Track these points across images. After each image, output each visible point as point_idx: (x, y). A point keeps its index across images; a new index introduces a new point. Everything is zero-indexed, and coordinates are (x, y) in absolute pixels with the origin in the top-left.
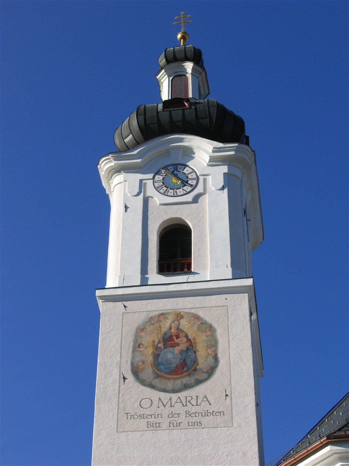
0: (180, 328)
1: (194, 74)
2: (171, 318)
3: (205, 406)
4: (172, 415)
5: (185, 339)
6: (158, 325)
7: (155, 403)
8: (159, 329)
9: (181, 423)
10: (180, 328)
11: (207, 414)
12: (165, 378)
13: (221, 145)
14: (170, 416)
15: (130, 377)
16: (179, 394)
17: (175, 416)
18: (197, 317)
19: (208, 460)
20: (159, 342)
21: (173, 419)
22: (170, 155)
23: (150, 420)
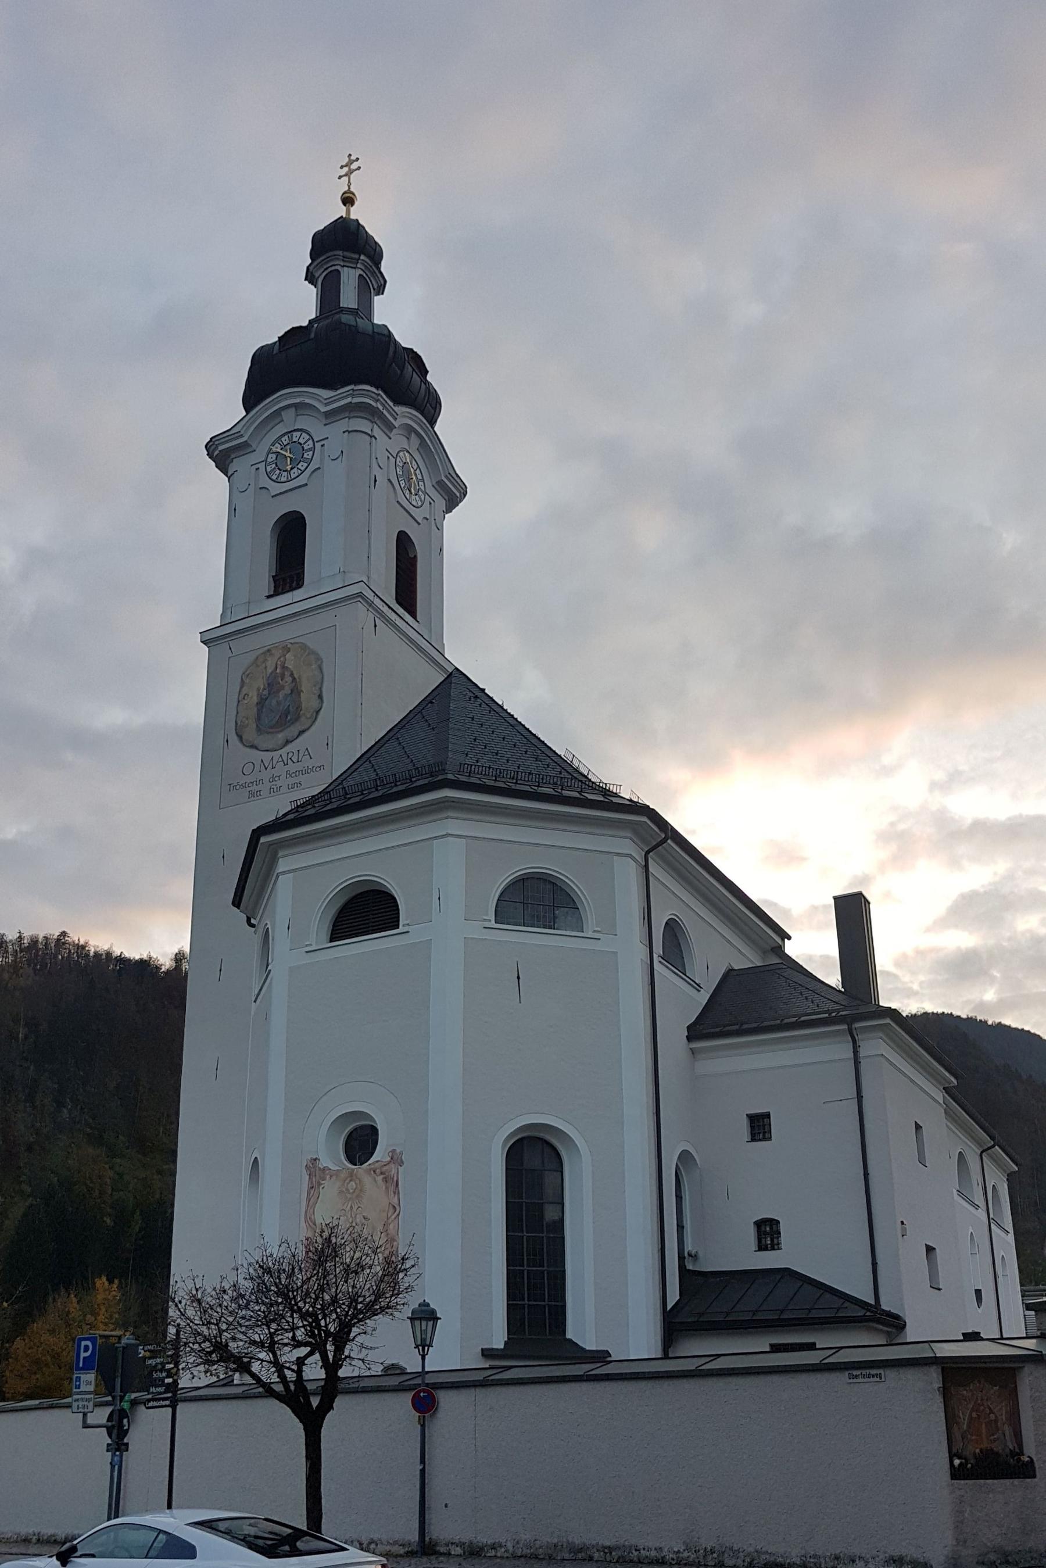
0: (286, 665)
1: (381, 292)
2: (277, 654)
3: (307, 763)
4: (273, 779)
5: (291, 679)
6: (264, 665)
7: (258, 764)
8: (264, 671)
9: (268, 597)
10: (286, 665)
11: (307, 771)
12: (268, 733)
13: (331, 393)
14: (271, 780)
15: (233, 738)
16: (280, 752)
17: (276, 779)
18: (304, 647)
19: (349, 1232)
20: (264, 689)
21: (274, 783)
22: (661, 1548)
23: (251, 789)
